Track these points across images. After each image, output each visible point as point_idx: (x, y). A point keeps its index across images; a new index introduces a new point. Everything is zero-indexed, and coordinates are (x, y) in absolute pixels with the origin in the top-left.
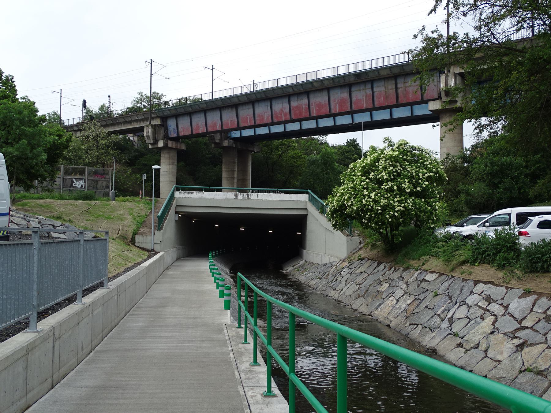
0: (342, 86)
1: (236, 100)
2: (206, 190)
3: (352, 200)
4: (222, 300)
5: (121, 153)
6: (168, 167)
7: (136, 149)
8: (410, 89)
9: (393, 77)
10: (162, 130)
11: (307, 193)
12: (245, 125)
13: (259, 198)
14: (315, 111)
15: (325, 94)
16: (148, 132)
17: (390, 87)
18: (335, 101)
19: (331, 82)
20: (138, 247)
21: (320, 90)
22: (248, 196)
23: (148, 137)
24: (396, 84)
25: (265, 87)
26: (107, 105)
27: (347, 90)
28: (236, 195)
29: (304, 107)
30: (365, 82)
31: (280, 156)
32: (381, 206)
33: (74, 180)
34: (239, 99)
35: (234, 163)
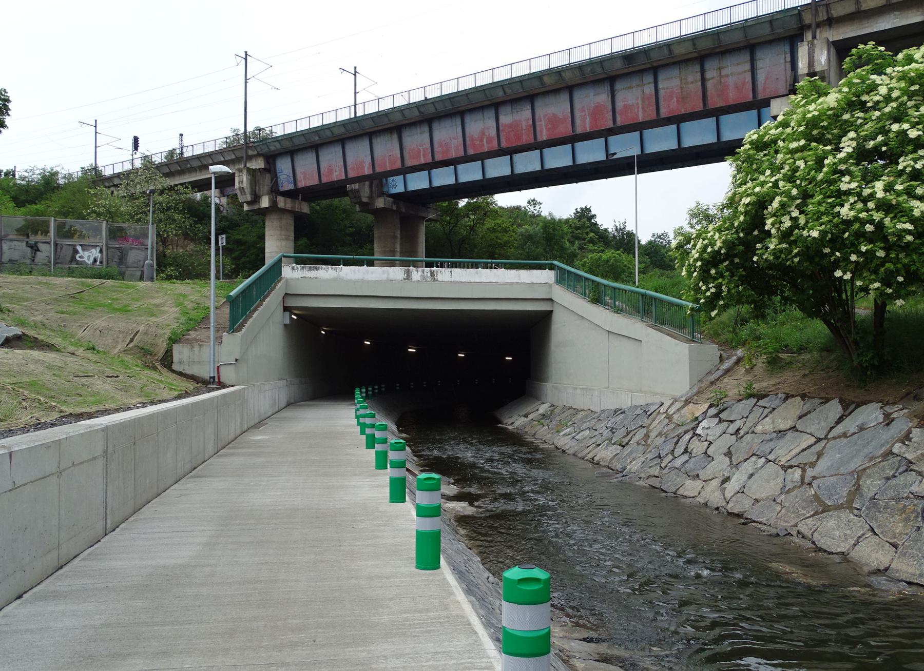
0: (596, 82)
1: (398, 118)
2: (347, 263)
3: (795, 213)
4: (372, 453)
5: (196, 223)
6: (279, 243)
7: (224, 217)
8: (731, 81)
9: (696, 58)
10: (268, 177)
11: (552, 267)
12: (416, 163)
13: (453, 279)
14: (544, 131)
15: (565, 97)
16: (242, 181)
17: (690, 79)
18: (583, 110)
19: (577, 73)
20: (181, 374)
21: (555, 91)
22: (432, 274)
23: (242, 190)
24: (703, 72)
25: (454, 89)
26: (178, 151)
27: (607, 88)
28: (408, 272)
29: (524, 124)
30: (641, 72)
31: (472, 228)
32: (913, 220)
33: (79, 248)
34: (403, 115)
35: (395, 237)
